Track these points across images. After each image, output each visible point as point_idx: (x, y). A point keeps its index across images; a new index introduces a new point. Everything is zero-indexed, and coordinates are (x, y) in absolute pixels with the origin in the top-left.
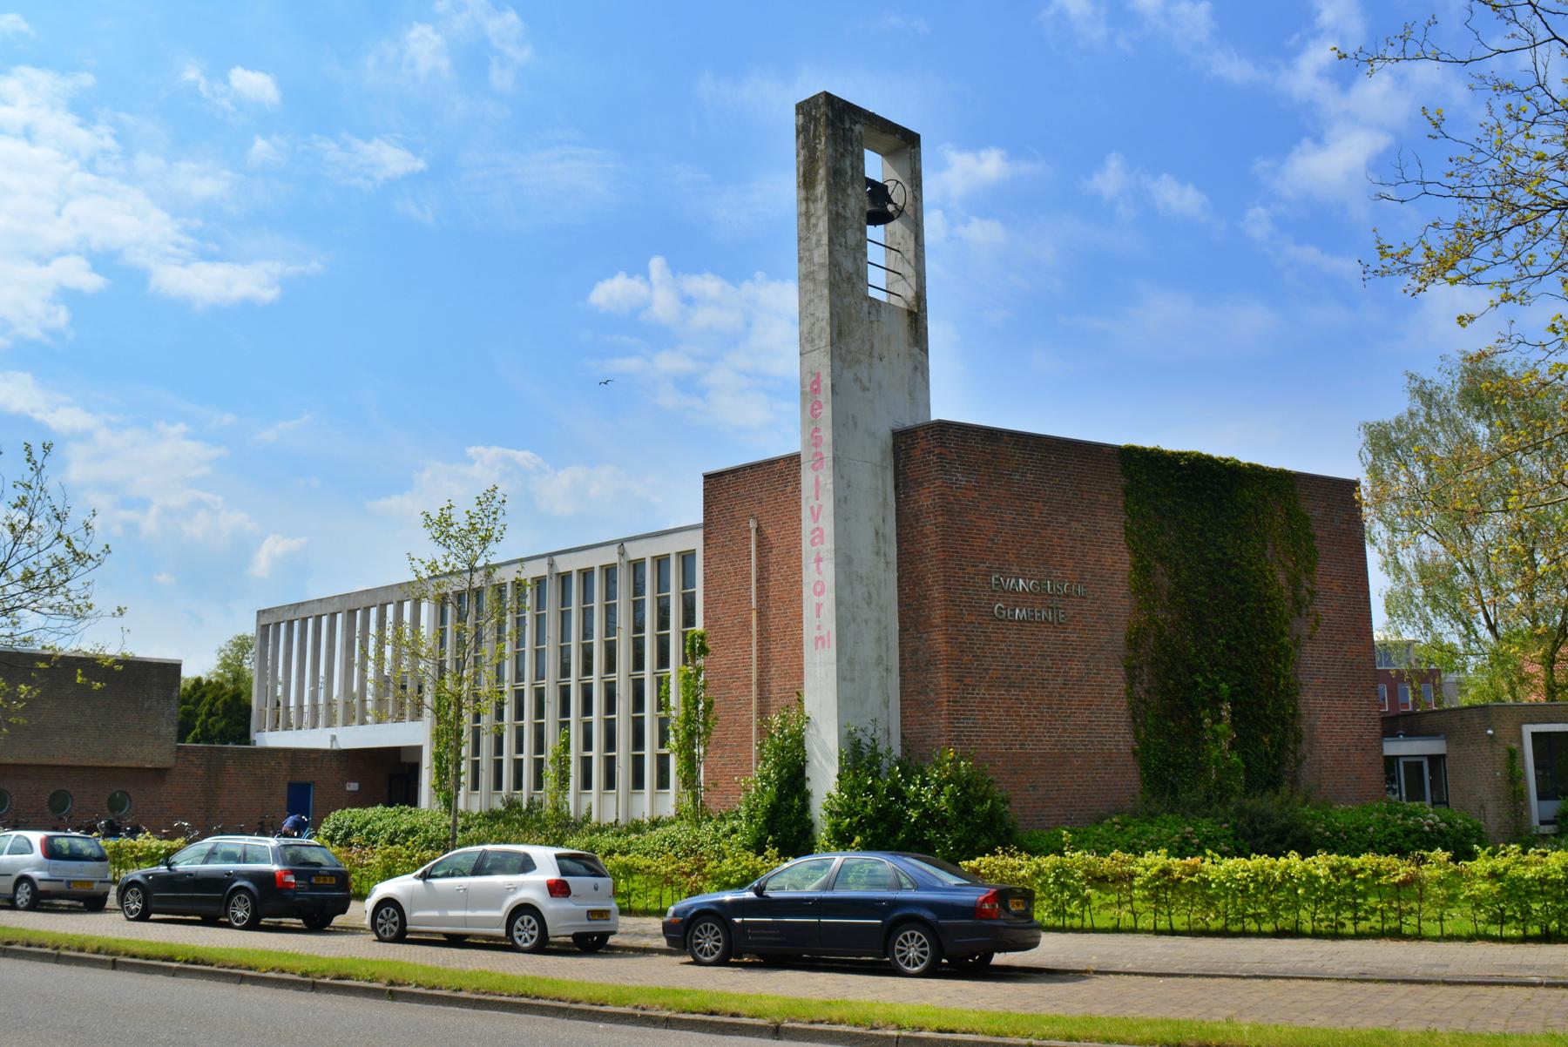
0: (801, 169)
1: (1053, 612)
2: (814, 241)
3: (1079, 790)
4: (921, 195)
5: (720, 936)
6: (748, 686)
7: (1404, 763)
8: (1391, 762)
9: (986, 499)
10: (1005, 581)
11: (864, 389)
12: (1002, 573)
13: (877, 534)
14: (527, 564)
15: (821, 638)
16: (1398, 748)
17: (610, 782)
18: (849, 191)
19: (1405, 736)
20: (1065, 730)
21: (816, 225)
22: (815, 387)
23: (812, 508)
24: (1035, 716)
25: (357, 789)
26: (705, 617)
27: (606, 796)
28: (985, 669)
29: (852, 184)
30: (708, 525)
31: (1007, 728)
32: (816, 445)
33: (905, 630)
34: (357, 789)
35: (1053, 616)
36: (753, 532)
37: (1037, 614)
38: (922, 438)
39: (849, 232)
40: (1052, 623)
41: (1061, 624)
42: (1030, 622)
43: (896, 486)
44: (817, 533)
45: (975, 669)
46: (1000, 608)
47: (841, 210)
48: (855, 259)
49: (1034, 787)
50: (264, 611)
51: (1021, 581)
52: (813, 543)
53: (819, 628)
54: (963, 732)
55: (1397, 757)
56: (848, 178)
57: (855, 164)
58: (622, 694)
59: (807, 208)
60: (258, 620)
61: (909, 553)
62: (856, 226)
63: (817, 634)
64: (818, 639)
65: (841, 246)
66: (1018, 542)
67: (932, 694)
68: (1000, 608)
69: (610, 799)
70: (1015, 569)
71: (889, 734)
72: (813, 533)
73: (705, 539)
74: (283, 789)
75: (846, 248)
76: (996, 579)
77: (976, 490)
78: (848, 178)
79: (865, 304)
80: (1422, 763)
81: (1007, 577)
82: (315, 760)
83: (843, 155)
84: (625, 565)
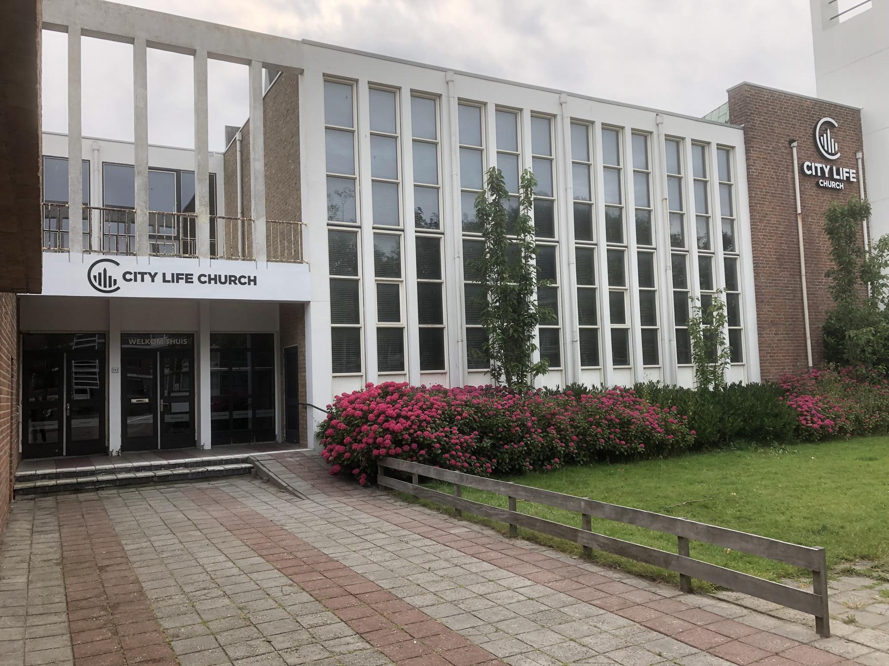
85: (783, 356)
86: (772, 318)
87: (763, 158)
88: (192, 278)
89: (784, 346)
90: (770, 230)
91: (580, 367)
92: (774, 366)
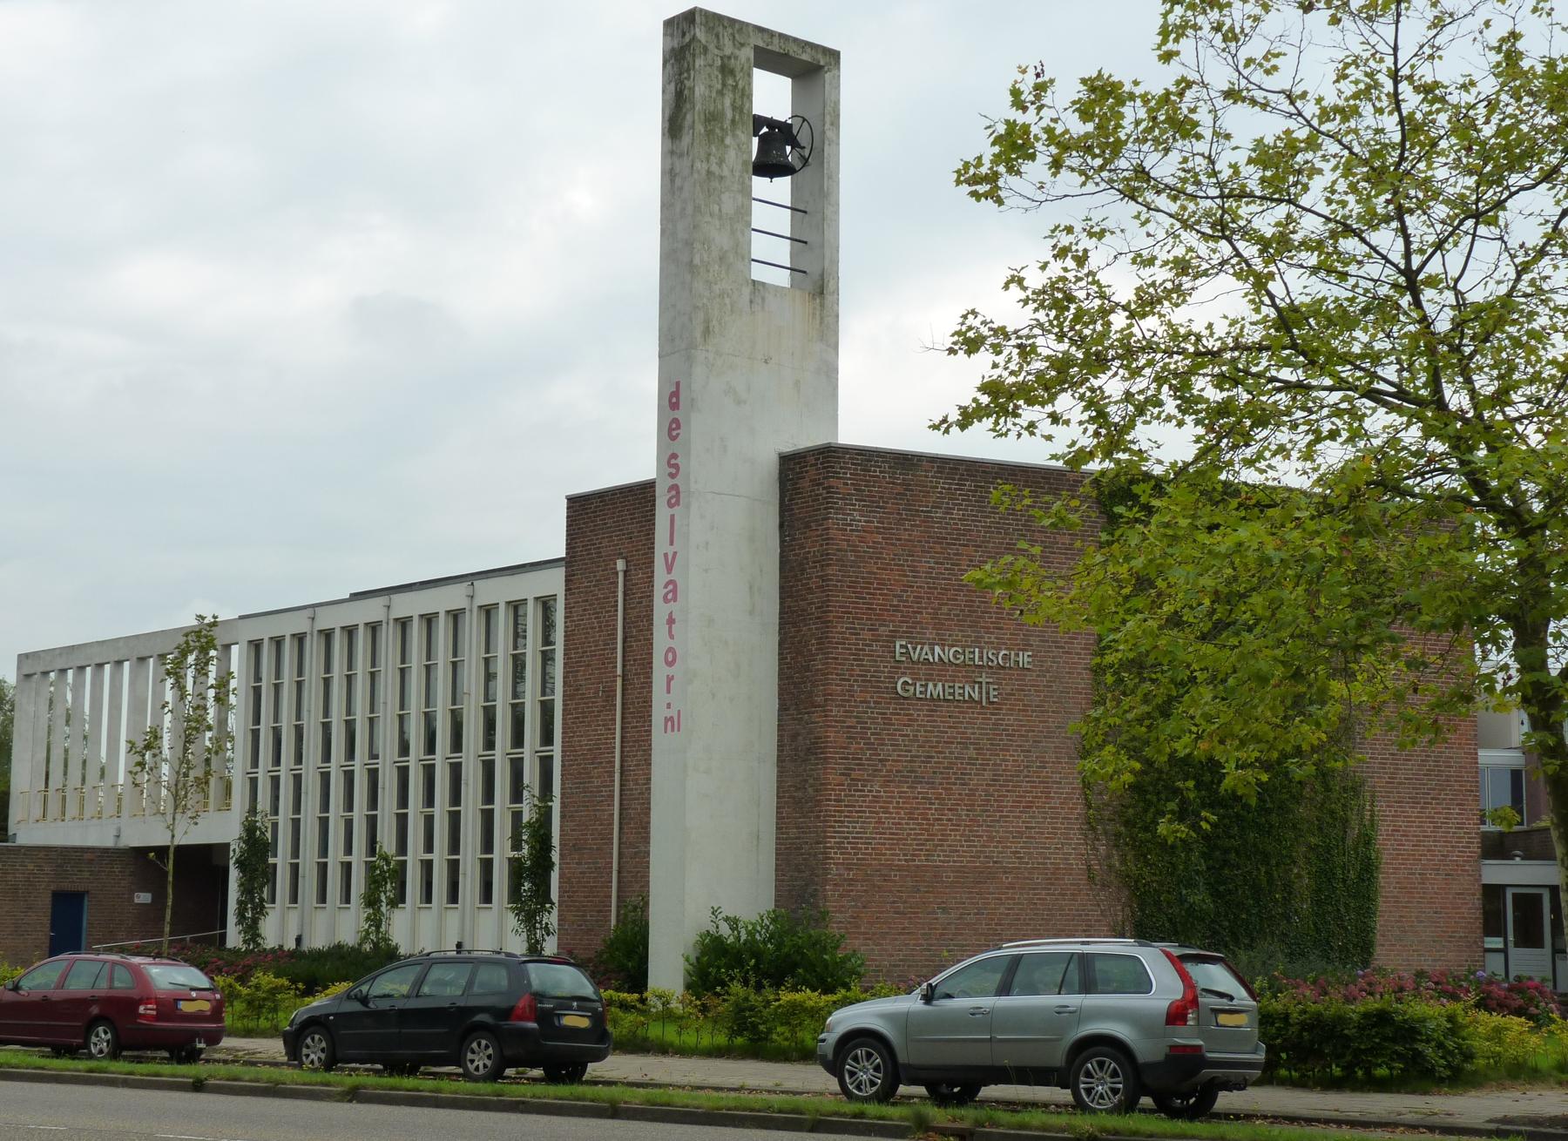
0: (667, 112)
1: (980, 688)
3: (1008, 914)
5: (490, 1051)
6: (612, 774)
7: (1514, 895)
8: (1493, 893)
9: (892, 544)
10: (915, 649)
11: (739, 402)
12: (911, 640)
13: (751, 588)
14: (396, 598)
16: (1498, 872)
18: (728, 141)
19: (1523, 858)
20: (991, 839)
21: (681, 189)
22: (674, 400)
23: (666, 555)
24: (949, 820)
26: (565, 683)
27: (422, 912)
28: (880, 760)
29: (733, 131)
32: (672, 476)
33: (786, 710)
35: (980, 693)
37: (958, 691)
39: (725, 197)
40: (980, 702)
44: (671, 587)
45: (868, 759)
46: (906, 683)
47: (714, 168)
48: (733, 232)
49: (944, 909)
50: (27, 656)
51: (937, 649)
52: (666, 600)
53: (669, 706)
54: (847, 838)
55: (1503, 888)
56: (727, 124)
57: (739, 102)
60: (19, 668)
62: (736, 187)
64: (667, 720)
65: (711, 215)
66: (936, 598)
67: (810, 790)
68: (906, 683)
69: (428, 919)
70: (930, 634)
72: (666, 587)
73: (568, 581)
74: (46, 901)
76: (901, 646)
78: (727, 124)
79: (746, 291)
80: (1540, 896)
81: (917, 643)
82: (91, 861)
83: (721, 93)
84: (475, 610)
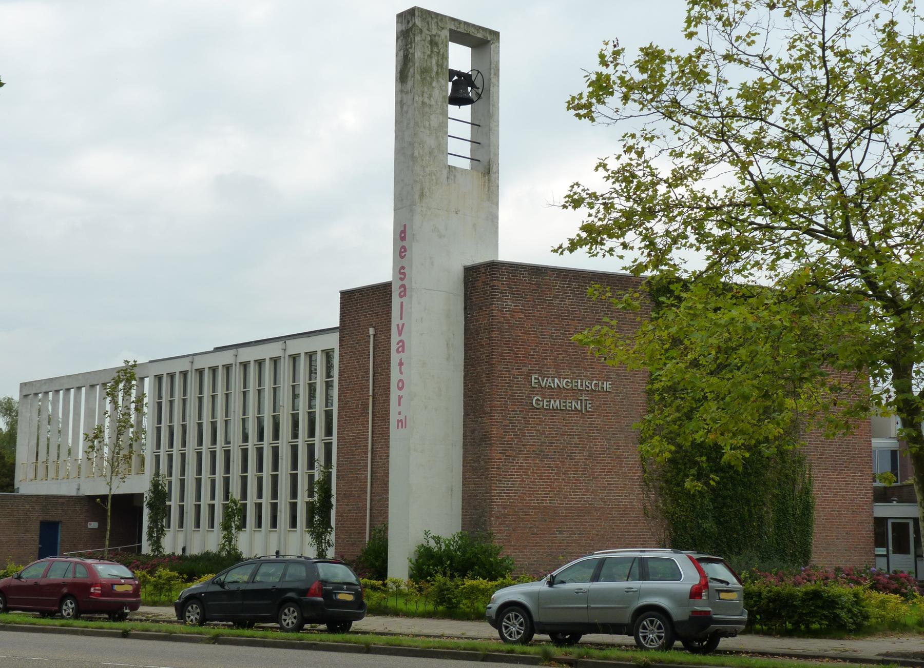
1: (581, 403)
2: (405, 124)
4: (498, 81)
7: (892, 523)
8: (880, 522)
10: (543, 380)
11: (441, 236)
15: (401, 421)
16: (882, 510)
17: (274, 524)
18: (434, 84)
20: (587, 490)
21: (407, 112)
22: (403, 235)
25: (97, 527)
28: (523, 445)
29: (437, 79)
30: (343, 329)
31: (540, 488)
32: (402, 279)
34: (97, 527)
35: (581, 406)
36: (372, 337)
37: (568, 404)
38: (483, 273)
39: (432, 117)
40: (581, 411)
41: (589, 411)
42: (561, 410)
43: (465, 308)
44: (401, 344)
46: (538, 400)
47: (426, 100)
48: (437, 137)
50: (25, 384)
52: (398, 352)
53: (400, 413)
54: (503, 490)
56: (434, 74)
57: (440, 62)
58: (284, 457)
59: (402, 98)
60: (21, 391)
61: (472, 359)
62: (439, 111)
63: (400, 418)
66: (556, 351)
67: (482, 463)
68: (538, 400)
69: (259, 537)
70: (552, 371)
71: (452, 490)
72: (398, 344)
73: (341, 341)
74: (35, 527)
75: (430, 129)
76: (535, 378)
77: (522, 312)
78: (434, 74)
79: (445, 172)
80: (907, 524)
81: (545, 377)
82: (62, 504)
83: (430, 56)
85: (351, 524)
86: (345, 491)
87: (350, 352)
88: (402, 427)
89: (353, 516)
90: (350, 415)
91: (207, 529)
92: (343, 533)
